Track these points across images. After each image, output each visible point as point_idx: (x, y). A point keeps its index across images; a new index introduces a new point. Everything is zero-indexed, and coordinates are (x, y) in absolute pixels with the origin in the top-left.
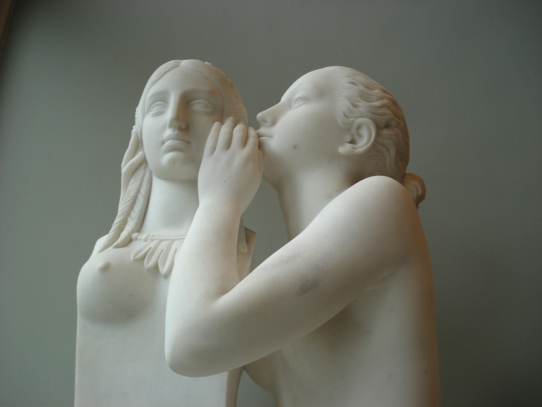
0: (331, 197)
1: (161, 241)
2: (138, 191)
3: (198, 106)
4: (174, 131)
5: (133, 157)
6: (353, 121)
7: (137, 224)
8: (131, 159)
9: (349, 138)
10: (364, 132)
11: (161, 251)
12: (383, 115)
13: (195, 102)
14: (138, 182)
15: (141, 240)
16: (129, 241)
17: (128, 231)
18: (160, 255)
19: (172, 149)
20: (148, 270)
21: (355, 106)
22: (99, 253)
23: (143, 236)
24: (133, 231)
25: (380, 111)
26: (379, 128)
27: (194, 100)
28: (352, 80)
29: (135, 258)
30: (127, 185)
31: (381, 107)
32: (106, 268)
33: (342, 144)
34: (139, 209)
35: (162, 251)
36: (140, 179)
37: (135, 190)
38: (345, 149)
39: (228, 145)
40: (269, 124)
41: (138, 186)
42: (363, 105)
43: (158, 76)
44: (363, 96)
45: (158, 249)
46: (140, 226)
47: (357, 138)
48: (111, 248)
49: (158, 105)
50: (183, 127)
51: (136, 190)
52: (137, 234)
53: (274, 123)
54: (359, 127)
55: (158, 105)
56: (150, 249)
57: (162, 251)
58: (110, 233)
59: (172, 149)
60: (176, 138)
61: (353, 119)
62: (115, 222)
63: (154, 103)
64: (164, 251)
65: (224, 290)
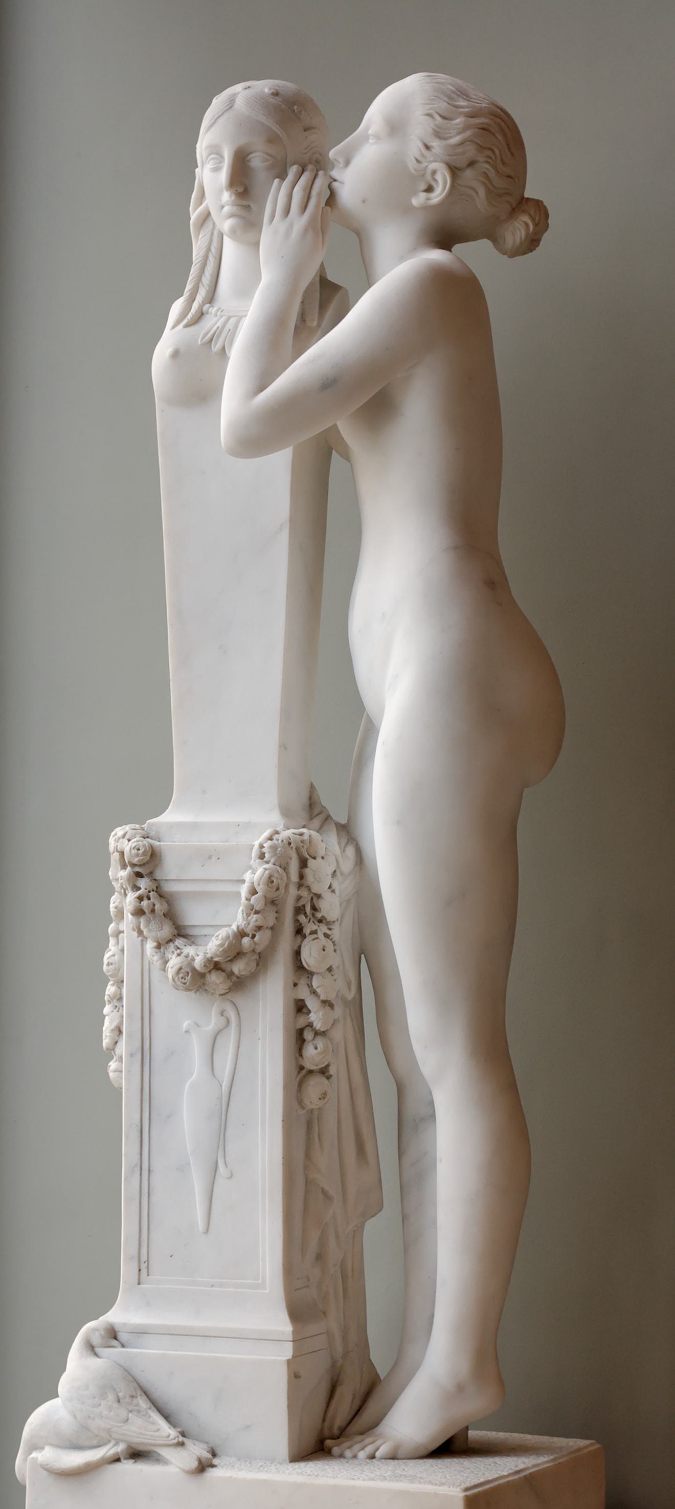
0: (402, 259)
1: (229, 318)
2: (209, 249)
3: (257, 162)
4: (231, 196)
5: (201, 204)
6: (427, 167)
7: (208, 292)
8: (199, 207)
9: (423, 186)
10: (439, 177)
11: (228, 330)
12: (463, 153)
13: (251, 156)
14: (208, 236)
15: (211, 313)
16: (201, 315)
17: (199, 302)
18: (226, 337)
19: (232, 215)
20: (215, 353)
21: (428, 147)
22: (171, 329)
23: (213, 310)
24: (203, 304)
25: (460, 150)
26: (454, 171)
27: (251, 153)
28: (429, 109)
29: (202, 342)
30: (197, 237)
31: (461, 144)
32: (176, 354)
33: (415, 193)
34: (210, 272)
35: (230, 330)
36: (210, 233)
37: (205, 247)
38: (418, 200)
39: (287, 211)
40: (341, 165)
41: (208, 241)
42: (436, 144)
43: (211, 120)
44: (438, 134)
45: (225, 329)
46: (211, 298)
47: (433, 183)
48: (181, 326)
49: (210, 160)
50: (241, 190)
51: (190, 292)
52: (208, 305)
53: (347, 163)
54: (434, 172)
55: (210, 160)
56: (218, 328)
57: (230, 330)
58: (192, 275)
59: (232, 215)
60: (235, 204)
61: (426, 164)
62: (191, 273)
63: (209, 156)
64: (230, 331)
65: (261, 388)
